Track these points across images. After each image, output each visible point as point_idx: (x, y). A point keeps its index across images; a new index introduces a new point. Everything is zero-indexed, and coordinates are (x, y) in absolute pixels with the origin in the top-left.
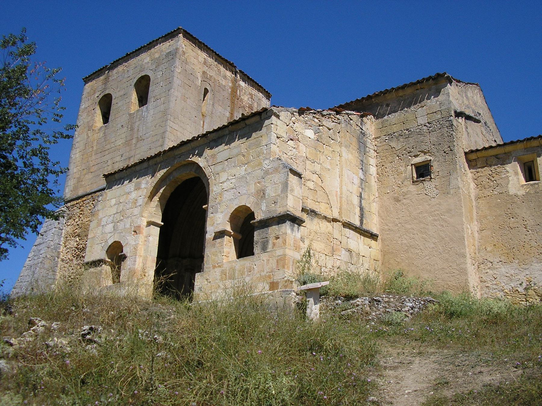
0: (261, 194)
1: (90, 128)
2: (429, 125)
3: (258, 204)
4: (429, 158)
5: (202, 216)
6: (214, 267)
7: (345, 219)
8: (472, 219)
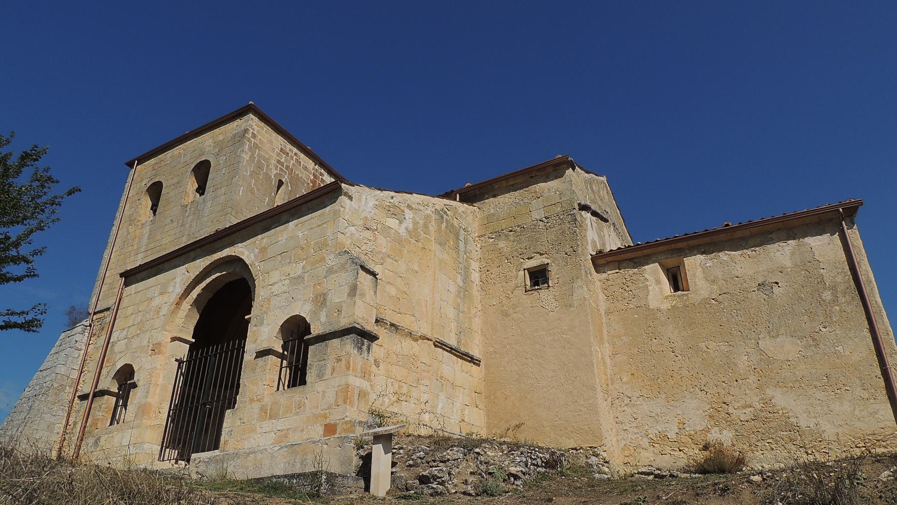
0: (321, 300)
1: (132, 221)
2: (546, 221)
3: (315, 313)
4: (546, 261)
5: (241, 332)
6: (252, 401)
7: (436, 336)
8: (602, 339)
